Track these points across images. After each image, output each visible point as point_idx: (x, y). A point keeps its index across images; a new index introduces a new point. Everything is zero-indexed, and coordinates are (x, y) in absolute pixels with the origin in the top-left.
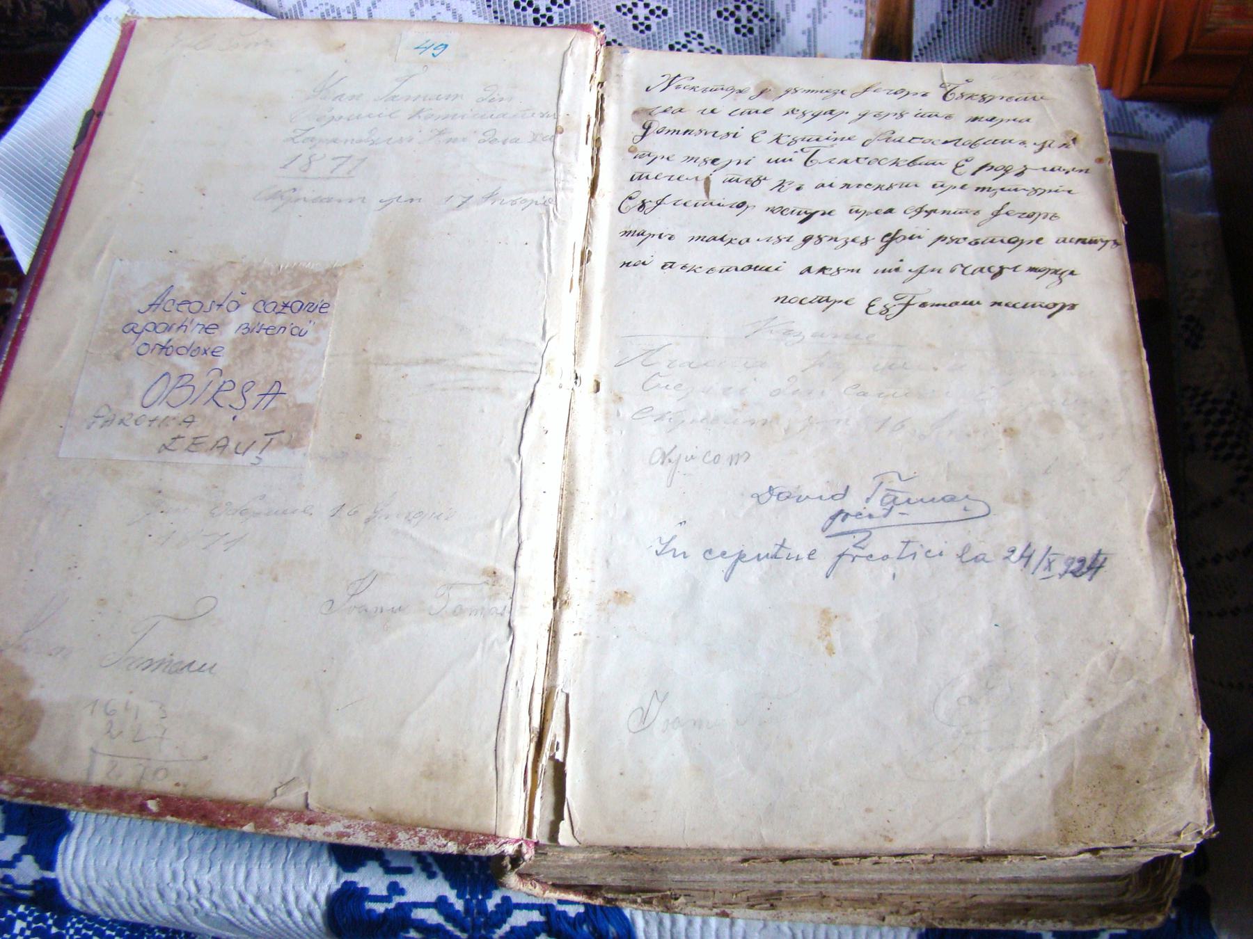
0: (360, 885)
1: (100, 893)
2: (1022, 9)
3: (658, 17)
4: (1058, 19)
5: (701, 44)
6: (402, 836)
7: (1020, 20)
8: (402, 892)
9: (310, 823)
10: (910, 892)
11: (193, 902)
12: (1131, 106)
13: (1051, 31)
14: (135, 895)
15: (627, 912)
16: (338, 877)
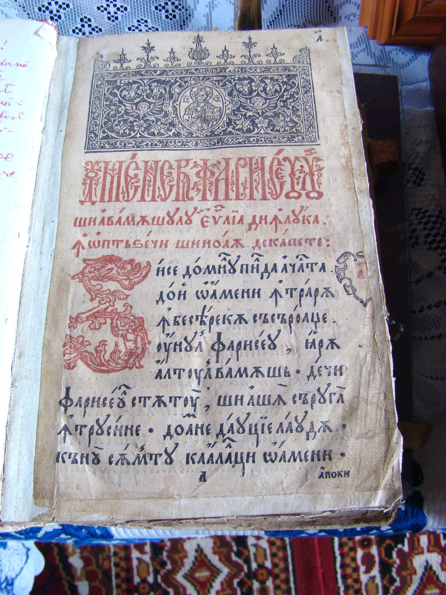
5: (146, 26)
12: (388, 48)
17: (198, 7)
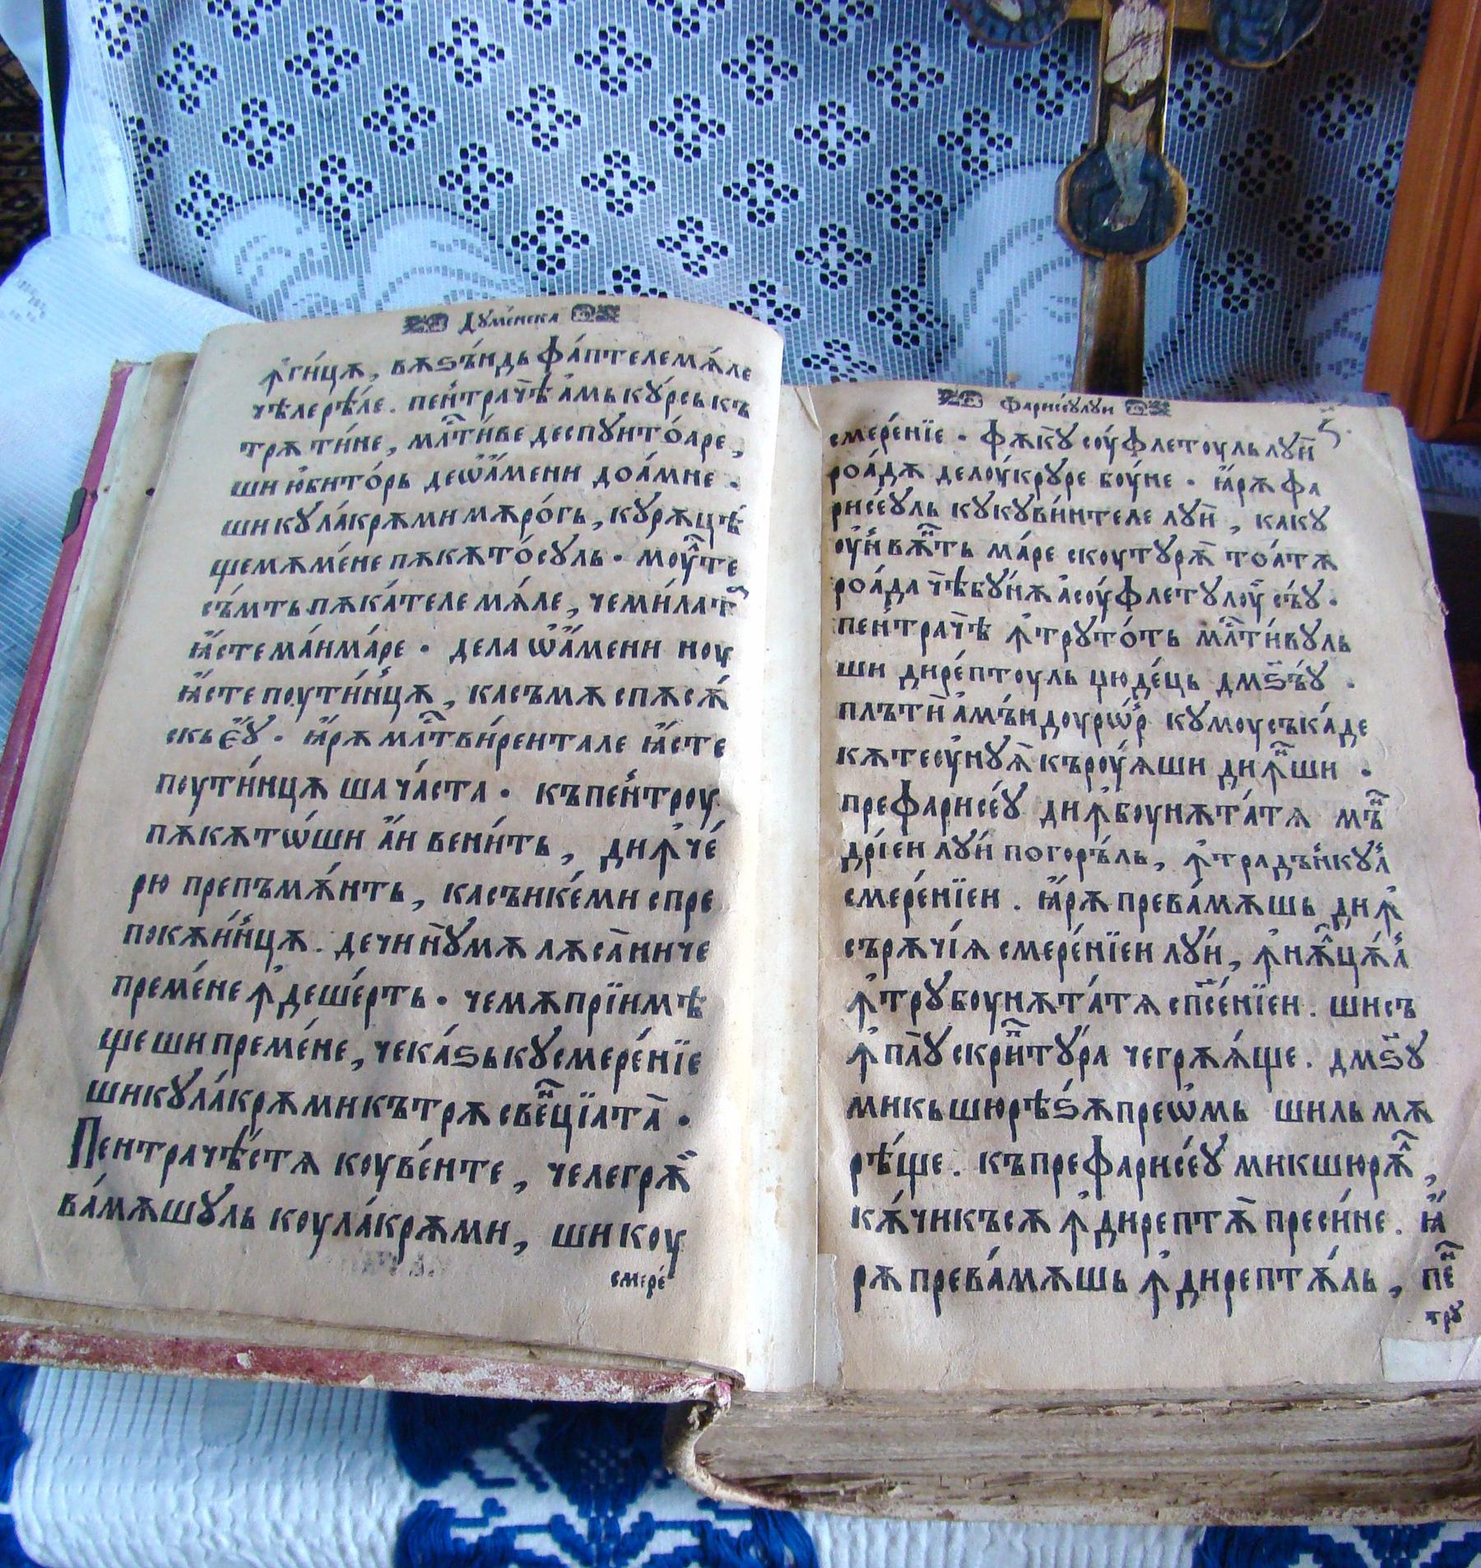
0: (444, 1505)
1: (72, 1532)
2: (1289, 313)
3: (787, 319)
4: (1338, 327)
5: (847, 358)
6: (563, 1381)
7: (1286, 328)
8: (502, 1511)
9: (445, 1370)
10: (1193, 1469)
11: (207, 1541)
12: (1437, 449)
13: (1328, 344)
14: (122, 1532)
15: (809, 1528)
16: (412, 1495)
17: (975, 321)
